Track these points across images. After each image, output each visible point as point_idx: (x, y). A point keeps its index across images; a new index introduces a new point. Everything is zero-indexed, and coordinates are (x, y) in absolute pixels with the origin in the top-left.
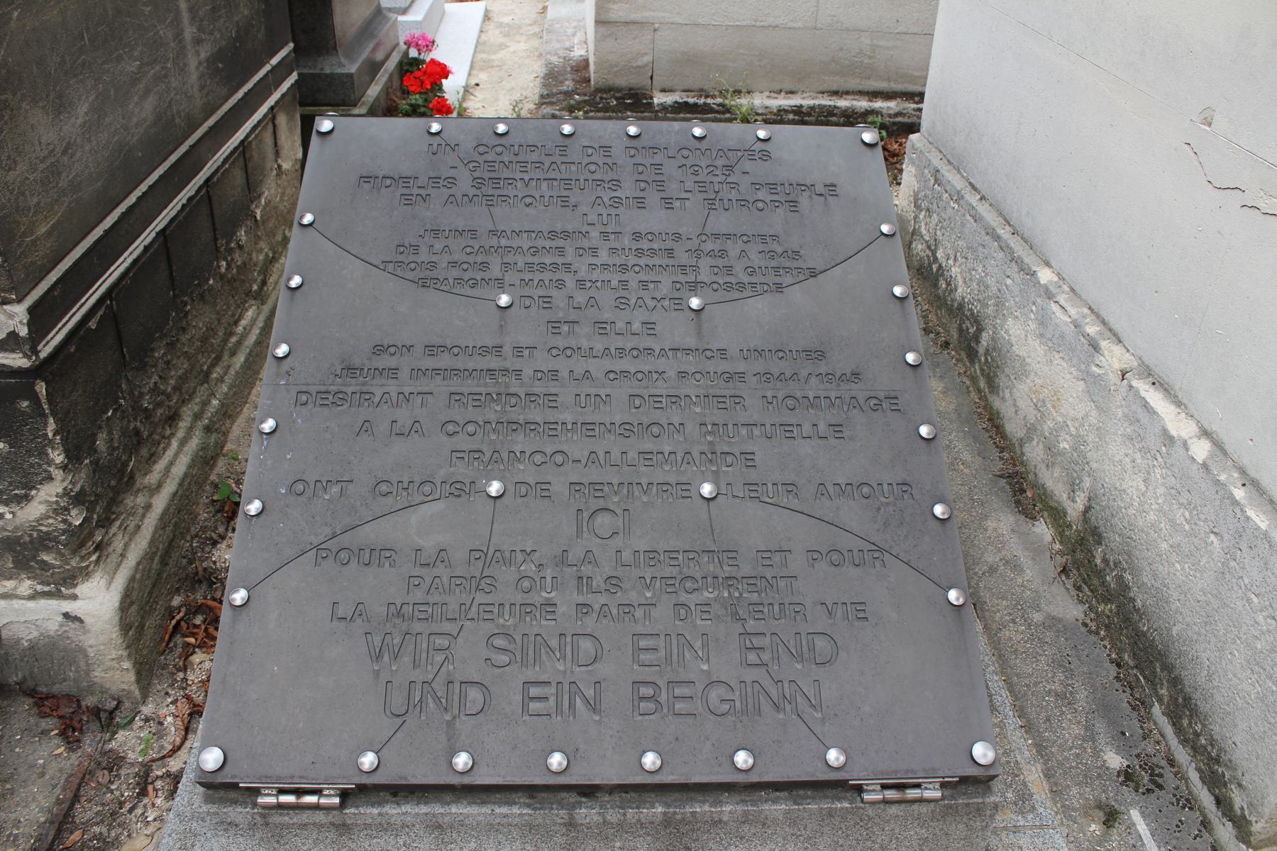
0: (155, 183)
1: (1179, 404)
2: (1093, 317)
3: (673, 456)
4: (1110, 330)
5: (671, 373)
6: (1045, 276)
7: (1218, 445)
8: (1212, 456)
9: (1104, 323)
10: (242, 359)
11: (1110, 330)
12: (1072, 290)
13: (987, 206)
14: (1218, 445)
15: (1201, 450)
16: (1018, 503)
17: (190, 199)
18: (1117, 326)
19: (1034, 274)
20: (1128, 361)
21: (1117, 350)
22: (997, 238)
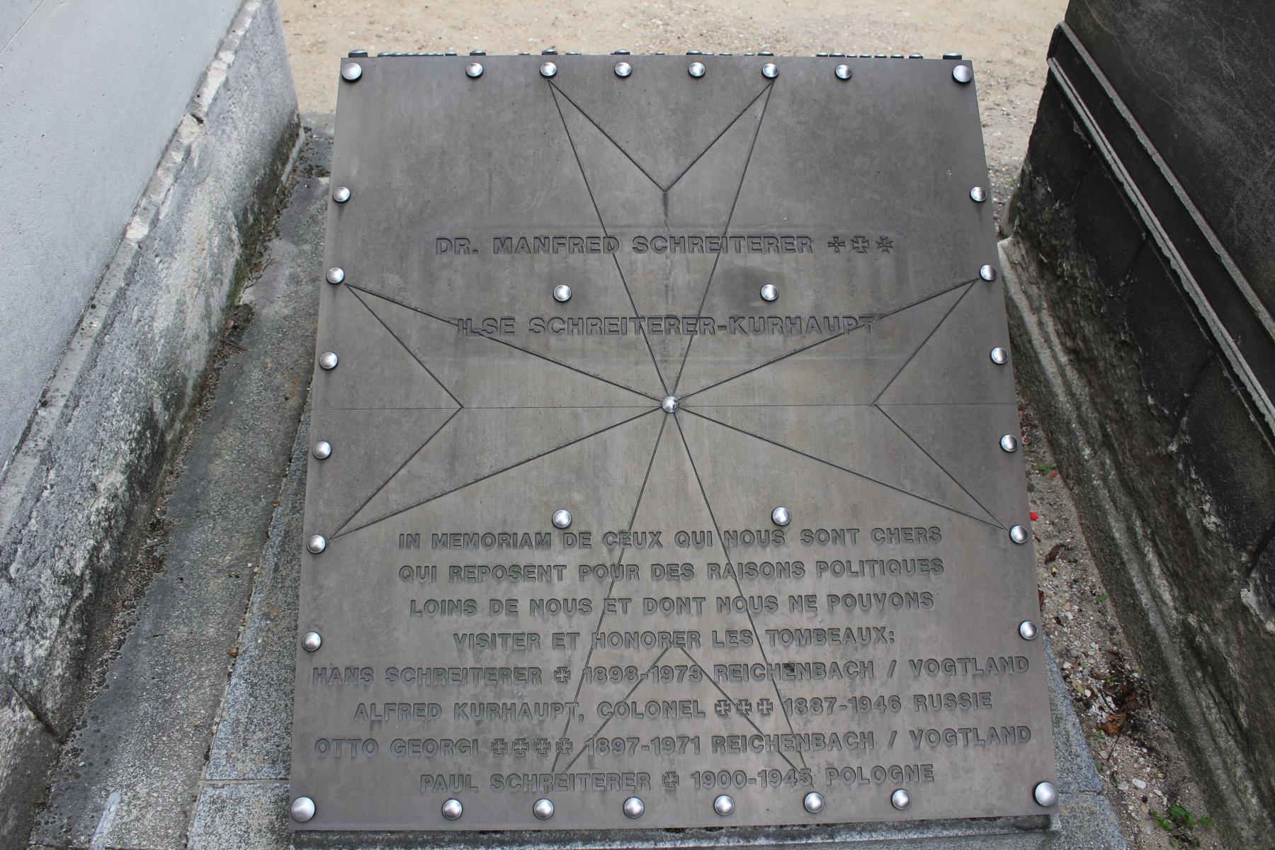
0: (1114, 106)
1: (205, 75)
2: (164, 163)
3: (508, 241)
4: (171, 141)
5: (483, 602)
6: (138, 231)
7: (221, 46)
8: (226, 49)
9: (167, 148)
10: (1117, 535)
11: (171, 141)
12: (144, 194)
13: (57, 383)
14: (221, 46)
15: (227, 56)
16: (247, 320)
17: (1167, 260)
18: (169, 134)
19: (140, 245)
20: (189, 121)
21: (184, 131)
22: (107, 327)
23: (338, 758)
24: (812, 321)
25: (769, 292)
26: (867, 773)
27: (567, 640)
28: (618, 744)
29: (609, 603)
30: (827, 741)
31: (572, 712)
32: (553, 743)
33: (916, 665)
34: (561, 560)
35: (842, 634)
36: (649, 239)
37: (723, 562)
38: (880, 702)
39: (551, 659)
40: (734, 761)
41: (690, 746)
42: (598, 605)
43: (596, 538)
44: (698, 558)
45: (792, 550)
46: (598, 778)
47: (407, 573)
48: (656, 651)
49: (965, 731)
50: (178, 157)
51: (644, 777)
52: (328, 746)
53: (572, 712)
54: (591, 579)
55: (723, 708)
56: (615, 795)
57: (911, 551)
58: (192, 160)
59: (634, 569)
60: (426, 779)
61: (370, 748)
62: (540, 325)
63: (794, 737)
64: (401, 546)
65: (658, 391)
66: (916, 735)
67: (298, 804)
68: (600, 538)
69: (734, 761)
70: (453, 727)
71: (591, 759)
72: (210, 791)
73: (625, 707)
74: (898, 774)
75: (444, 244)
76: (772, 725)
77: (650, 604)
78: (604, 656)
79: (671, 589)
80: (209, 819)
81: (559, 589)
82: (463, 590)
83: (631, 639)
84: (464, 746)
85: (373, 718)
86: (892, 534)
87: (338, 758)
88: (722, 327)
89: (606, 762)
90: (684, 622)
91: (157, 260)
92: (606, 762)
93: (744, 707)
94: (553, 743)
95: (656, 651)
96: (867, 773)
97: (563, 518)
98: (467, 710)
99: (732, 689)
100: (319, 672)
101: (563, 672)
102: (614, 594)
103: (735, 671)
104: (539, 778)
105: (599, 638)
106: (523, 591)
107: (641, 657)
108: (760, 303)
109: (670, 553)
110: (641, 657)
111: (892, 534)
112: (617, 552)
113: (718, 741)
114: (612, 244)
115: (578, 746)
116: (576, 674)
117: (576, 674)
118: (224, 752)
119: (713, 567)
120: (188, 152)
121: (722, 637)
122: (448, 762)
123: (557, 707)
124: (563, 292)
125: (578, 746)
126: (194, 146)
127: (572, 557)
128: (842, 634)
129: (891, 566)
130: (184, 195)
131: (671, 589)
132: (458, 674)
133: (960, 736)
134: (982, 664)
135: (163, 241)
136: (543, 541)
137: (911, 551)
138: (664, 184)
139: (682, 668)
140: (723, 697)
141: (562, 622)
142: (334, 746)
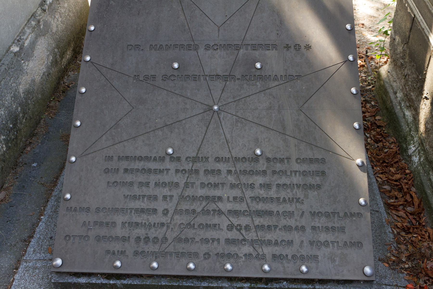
23: (73, 243)
24: (276, 77)
25: (258, 65)
26: (290, 257)
27: (168, 199)
28: (187, 240)
29: (187, 185)
30: (273, 243)
31: (168, 227)
32: (160, 240)
33: (313, 214)
34: (168, 167)
35: (281, 200)
36: (211, 45)
37: (233, 169)
38: (297, 228)
39: (160, 206)
40: (233, 249)
41: (216, 243)
42: (182, 185)
43: (183, 159)
44: (223, 167)
45: (262, 165)
46: (177, 254)
47: (107, 171)
48: (204, 204)
49: (333, 242)
50: (33, 23)
51: (196, 255)
52: (70, 239)
53: (168, 227)
54: (180, 174)
55: (230, 227)
56: (184, 261)
57: (314, 167)
58: (40, 26)
59: (197, 172)
60: (108, 252)
61: (87, 239)
62: (165, 78)
63: (259, 240)
64: (105, 161)
65: (211, 103)
66: (311, 243)
67: (56, 260)
68: (184, 159)
69: (233, 249)
70: (119, 231)
71: (174, 246)
72: (25, 264)
73: (190, 225)
74: (303, 259)
75: (130, 47)
76: (252, 235)
77: (203, 185)
78: (184, 206)
79: (212, 179)
80: (23, 274)
81: (166, 178)
82: (129, 178)
83: (194, 198)
84: (125, 239)
85: (89, 227)
86: (304, 160)
87: (73, 243)
88: (238, 79)
89: (181, 247)
90: (217, 193)
91: (23, 62)
92: (181, 247)
93: (239, 228)
94: (160, 240)
95: (204, 204)
96: (290, 257)
97: (170, 151)
98: (127, 225)
99: (235, 221)
100: (69, 209)
101: (166, 212)
102: (188, 181)
103: (236, 213)
104: (153, 253)
105: (182, 198)
106: (153, 178)
107: (198, 207)
108: (254, 70)
109: (212, 165)
110: (198, 207)
111: (304, 160)
112: (191, 165)
113: (228, 241)
114: (196, 48)
115: (170, 241)
116: (171, 212)
117: (171, 212)
118: (32, 249)
119: (229, 172)
120: (39, 22)
121: (231, 199)
122: (117, 246)
123: (163, 224)
124: (176, 65)
125: (170, 241)
126: (41, 20)
127: (172, 166)
128: (281, 200)
129: (304, 174)
130: (36, 38)
131: (212, 179)
132: (123, 211)
133: (331, 245)
134: (342, 214)
135: (25, 54)
136: (162, 159)
137: (314, 167)
138: (219, 25)
139: (214, 211)
140: (230, 223)
141: (166, 191)
142: (72, 238)
